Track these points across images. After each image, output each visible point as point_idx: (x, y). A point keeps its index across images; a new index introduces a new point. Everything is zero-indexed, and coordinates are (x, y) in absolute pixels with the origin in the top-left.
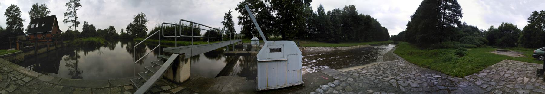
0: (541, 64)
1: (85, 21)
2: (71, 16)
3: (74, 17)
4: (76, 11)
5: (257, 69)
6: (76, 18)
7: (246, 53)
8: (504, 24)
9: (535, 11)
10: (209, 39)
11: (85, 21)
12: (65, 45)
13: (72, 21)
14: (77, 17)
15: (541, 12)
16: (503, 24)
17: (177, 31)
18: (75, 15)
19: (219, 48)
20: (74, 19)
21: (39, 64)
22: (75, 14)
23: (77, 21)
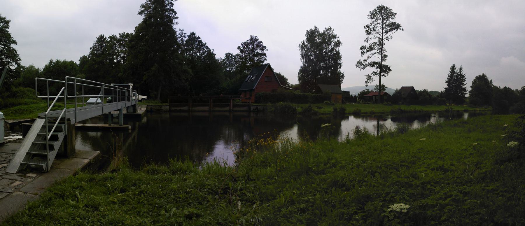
0: (381, 124)
1: (454, 66)
2: (373, 54)
3: (380, 56)
4: (385, 42)
5: (218, 144)
6: (382, 57)
7: (14, 122)
8: (54, 61)
9: (101, 35)
10: (76, 98)
11: (454, 66)
12: (252, 108)
13: (372, 64)
14: (386, 56)
15: (110, 37)
16: (51, 62)
17: (258, 81)
18: (381, 51)
19: (102, 114)
20: (377, 58)
21: (425, 139)
22: (382, 48)
23: (384, 63)
